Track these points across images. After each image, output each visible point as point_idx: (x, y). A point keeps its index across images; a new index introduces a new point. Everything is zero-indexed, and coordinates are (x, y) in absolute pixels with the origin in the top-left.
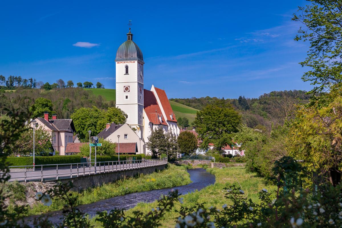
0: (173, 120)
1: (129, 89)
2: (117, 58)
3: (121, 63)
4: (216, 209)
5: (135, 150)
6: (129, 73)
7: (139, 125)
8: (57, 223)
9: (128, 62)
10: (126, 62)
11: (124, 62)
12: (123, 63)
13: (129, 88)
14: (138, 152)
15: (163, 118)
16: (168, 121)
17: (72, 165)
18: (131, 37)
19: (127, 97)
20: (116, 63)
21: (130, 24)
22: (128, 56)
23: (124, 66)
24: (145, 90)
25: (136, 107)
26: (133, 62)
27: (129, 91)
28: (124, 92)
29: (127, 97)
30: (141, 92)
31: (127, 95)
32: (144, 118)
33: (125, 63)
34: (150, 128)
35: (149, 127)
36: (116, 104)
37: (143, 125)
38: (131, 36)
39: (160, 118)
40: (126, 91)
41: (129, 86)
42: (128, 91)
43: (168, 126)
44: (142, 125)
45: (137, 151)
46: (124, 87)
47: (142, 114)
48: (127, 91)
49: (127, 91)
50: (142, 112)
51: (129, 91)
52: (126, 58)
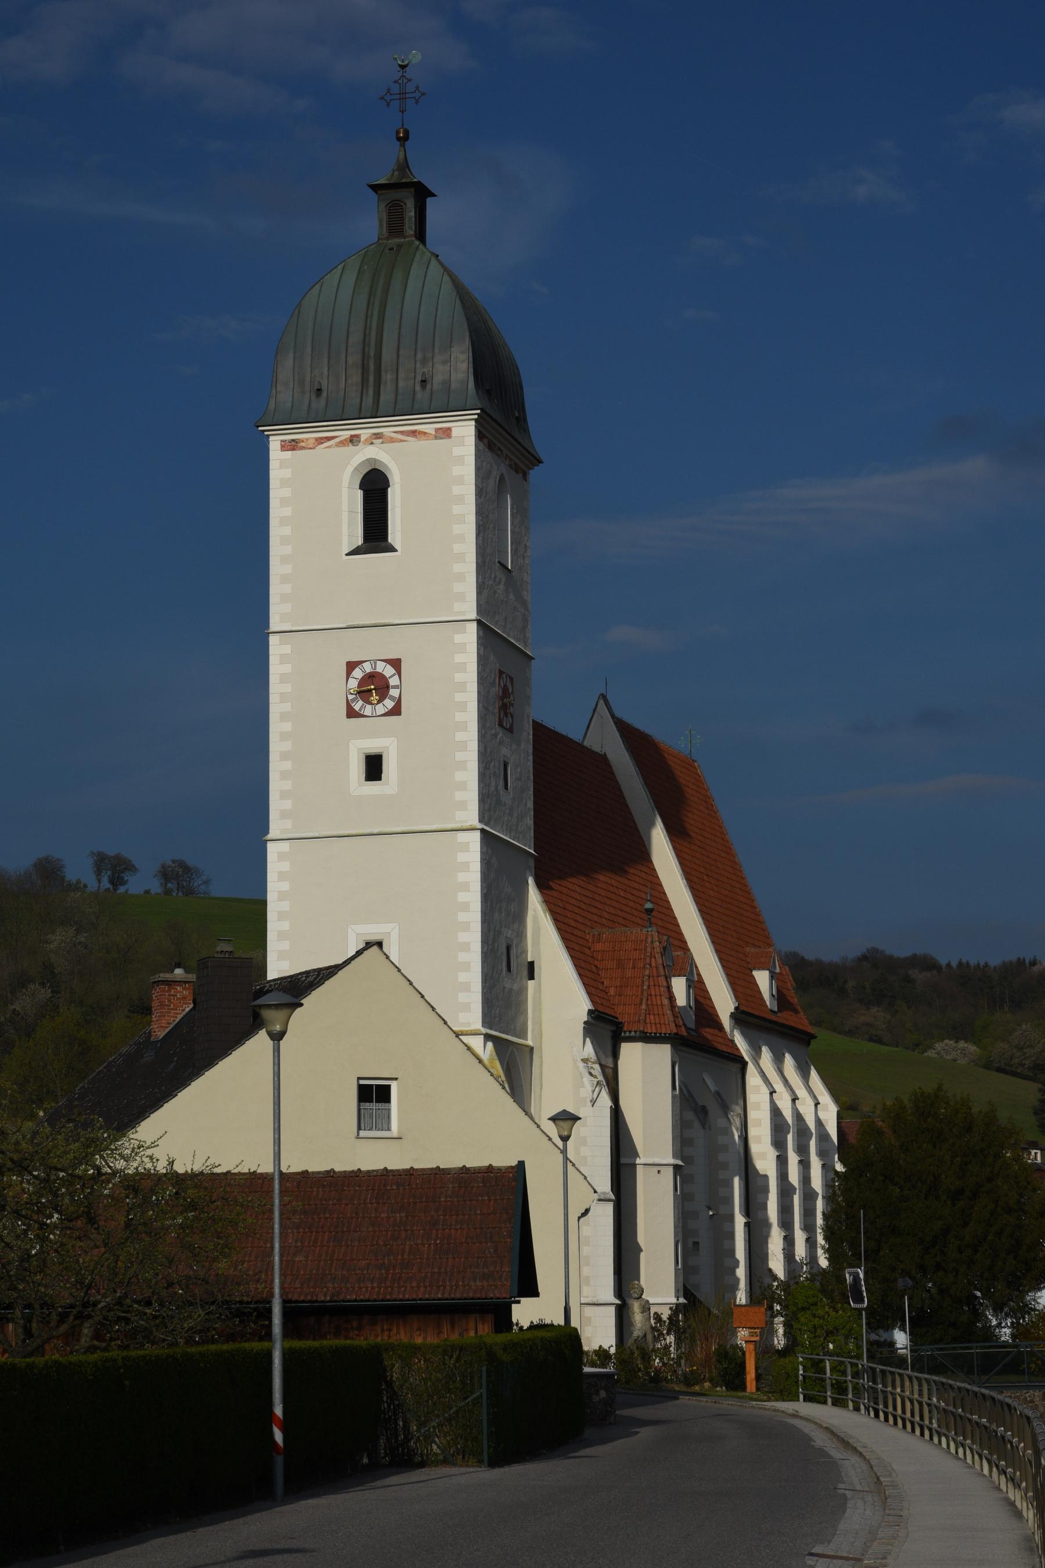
0: (787, 1018)
1: (394, 693)
2: (285, 396)
3: (320, 441)
4: (813, 1443)
5: (510, 1269)
6: (395, 534)
7: (488, 1037)
8: (654, 1350)
9: (387, 431)
10: (365, 434)
11: (346, 434)
12: (342, 443)
13: (394, 681)
14: (536, 1294)
15: (697, 986)
16: (739, 1017)
17: (860, 1310)
18: (411, 213)
19: (374, 767)
20: (275, 444)
21: (403, 96)
22: (388, 377)
23: (350, 469)
24: (539, 728)
25: (462, 857)
26: (430, 429)
27: (396, 711)
28: (351, 713)
29: (374, 767)
30: (507, 723)
31: (373, 750)
32: (542, 970)
33: (354, 440)
34: (597, 1069)
35: (585, 1061)
36: (267, 832)
37: (530, 1042)
38: (410, 205)
39: (679, 986)
40: (368, 710)
41: (396, 664)
42: (389, 704)
43: (744, 1064)
44: (523, 1035)
45: (529, 1287)
46: (351, 666)
47: (521, 934)
48: (380, 709)
49: (380, 709)
50: (519, 915)
51: (389, 661)
52: (369, 400)
